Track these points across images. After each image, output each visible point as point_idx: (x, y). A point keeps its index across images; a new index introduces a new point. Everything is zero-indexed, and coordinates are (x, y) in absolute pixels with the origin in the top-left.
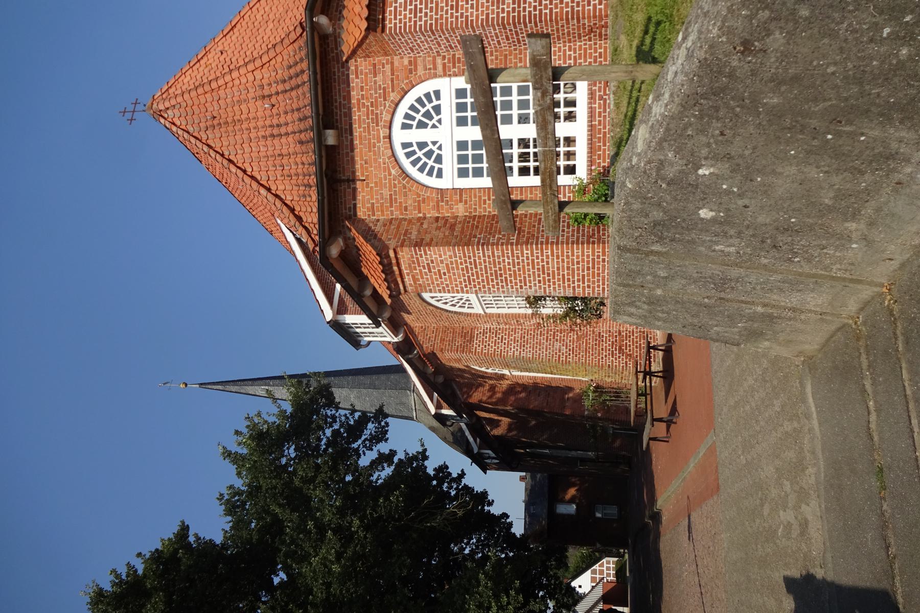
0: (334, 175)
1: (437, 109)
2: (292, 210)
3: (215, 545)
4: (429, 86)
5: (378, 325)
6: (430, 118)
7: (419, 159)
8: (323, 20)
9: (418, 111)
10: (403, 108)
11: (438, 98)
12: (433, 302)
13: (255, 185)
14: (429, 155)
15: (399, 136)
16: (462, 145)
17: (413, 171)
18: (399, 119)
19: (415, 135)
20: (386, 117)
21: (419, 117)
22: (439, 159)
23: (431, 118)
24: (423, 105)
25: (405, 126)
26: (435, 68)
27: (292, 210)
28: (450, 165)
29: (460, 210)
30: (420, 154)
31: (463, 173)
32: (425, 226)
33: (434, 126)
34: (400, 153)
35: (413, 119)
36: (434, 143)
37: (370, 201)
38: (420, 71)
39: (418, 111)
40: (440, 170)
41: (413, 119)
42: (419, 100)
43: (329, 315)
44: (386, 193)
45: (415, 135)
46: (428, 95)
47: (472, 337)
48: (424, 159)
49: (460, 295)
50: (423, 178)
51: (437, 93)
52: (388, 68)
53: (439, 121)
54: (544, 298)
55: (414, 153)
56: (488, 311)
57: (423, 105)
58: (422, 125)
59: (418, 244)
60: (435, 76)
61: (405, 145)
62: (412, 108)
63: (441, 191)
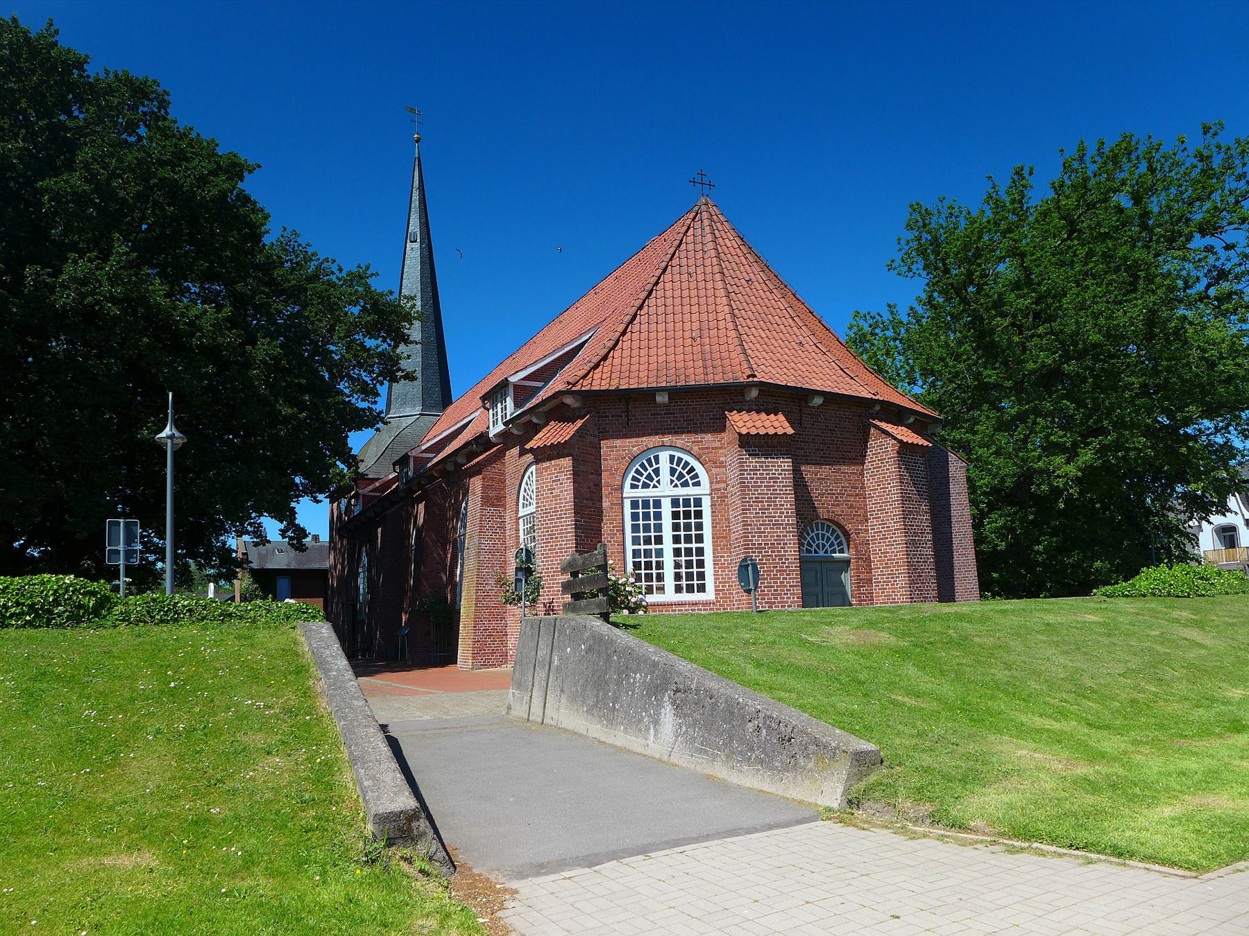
1: (685, 484)
3: (256, 237)
5: (506, 424)
6: (678, 479)
7: (646, 470)
9: (684, 468)
11: (694, 484)
12: (528, 473)
13: (628, 318)
14: (649, 477)
15: (628, 492)
19: (664, 466)
21: (679, 469)
23: (678, 479)
24: (688, 473)
26: (717, 482)
30: (650, 470)
31: (634, 504)
32: (591, 477)
33: (672, 481)
35: (678, 465)
36: (658, 482)
38: (714, 470)
39: (684, 468)
40: (637, 487)
41: (678, 465)
42: (692, 469)
45: (664, 466)
46: (696, 476)
47: (497, 506)
48: (645, 474)
49: (534, 497)
51: (698, 484)
52: (718, 444)
53: (676, 486)
55: (642, 475)
56: (521, 521)
57: (688, 473)
58: (673, 471)
60: (711, 483)
62: (687, 464)
63: (622, 488)
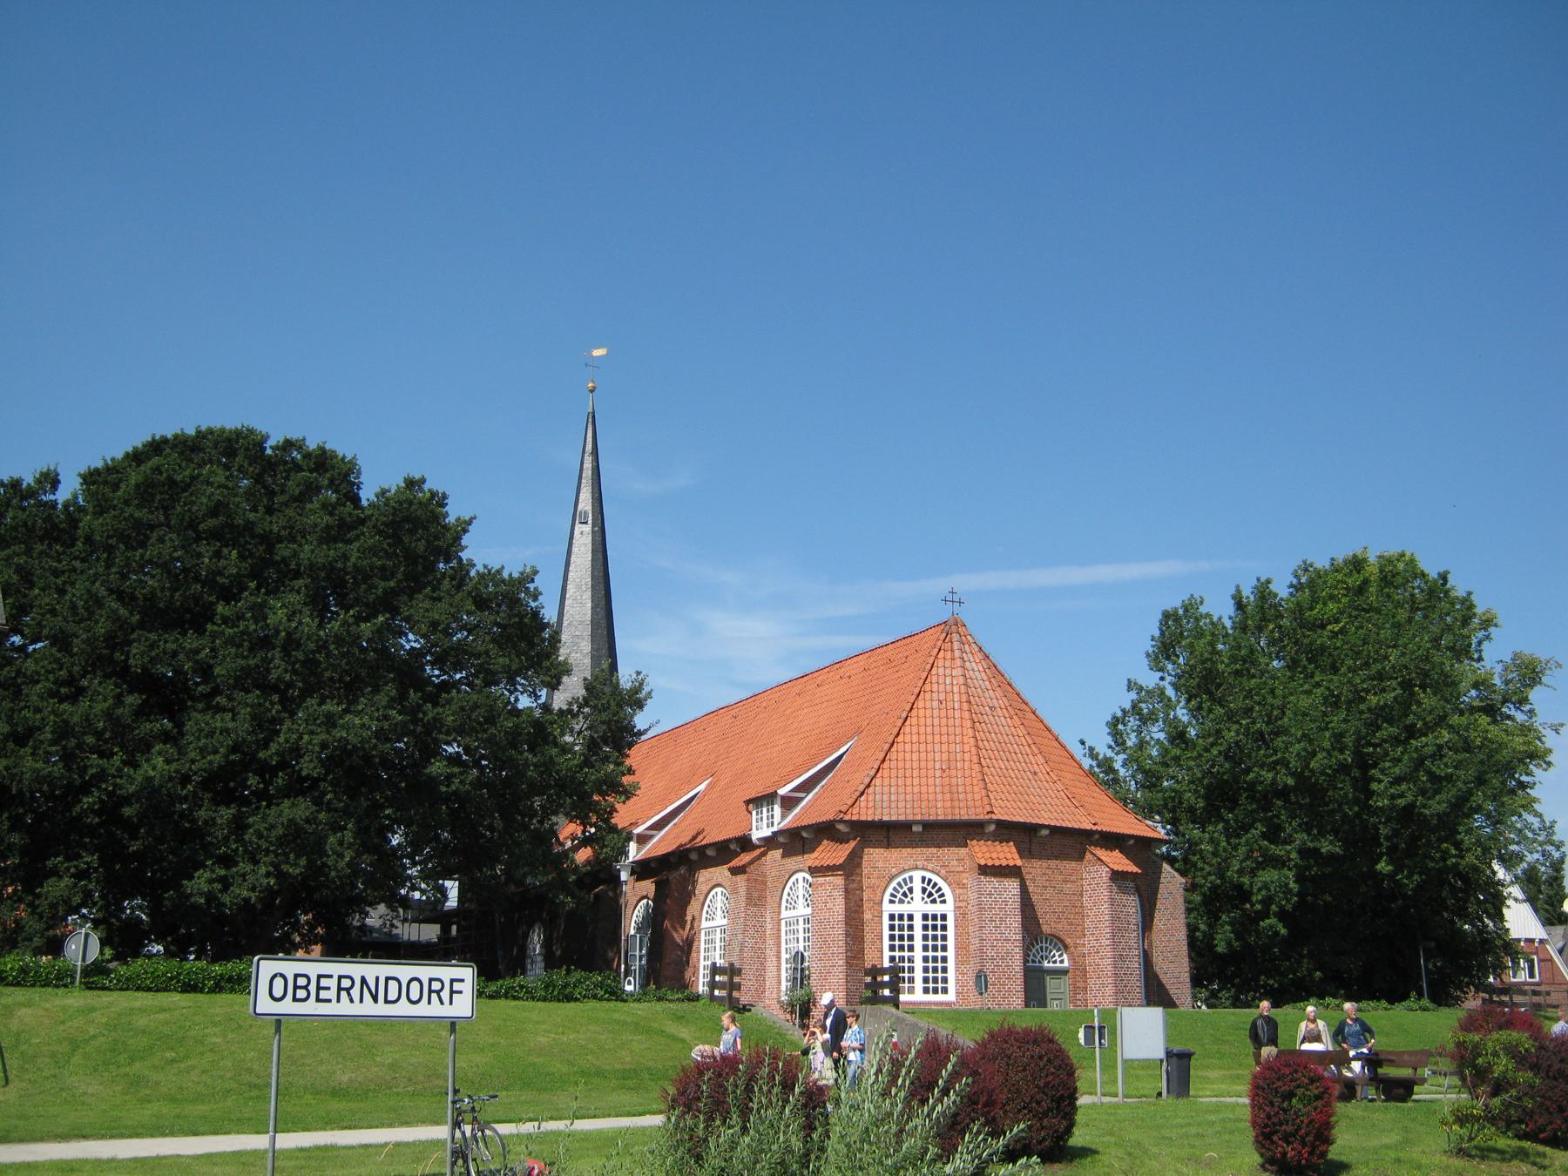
0: (891, 833)
1: (934, 901)
2: (868, 786)
4: (949, 896)
8: (992, 827)
10: (935, 878)
14: (905, 895)
15: (917, 875)
16: (911, 917)
17: (894, 884)
18: (928, 875)
20: (930, 866)
22: (901, 902)
25: (923, 879)
27: (868, 786)
28: (897, 908)
29: (867, 916)
31: (892, 917)
34: (906, 875)
37: (876, 858)
43: (782, 792)
44: (880, 864)
45: (917, 886)
50: (890, 890)
51: (944, 902)
54: (1066, 947)
58: (924, 890)
59: (847, 891)
61: (911, 878)
